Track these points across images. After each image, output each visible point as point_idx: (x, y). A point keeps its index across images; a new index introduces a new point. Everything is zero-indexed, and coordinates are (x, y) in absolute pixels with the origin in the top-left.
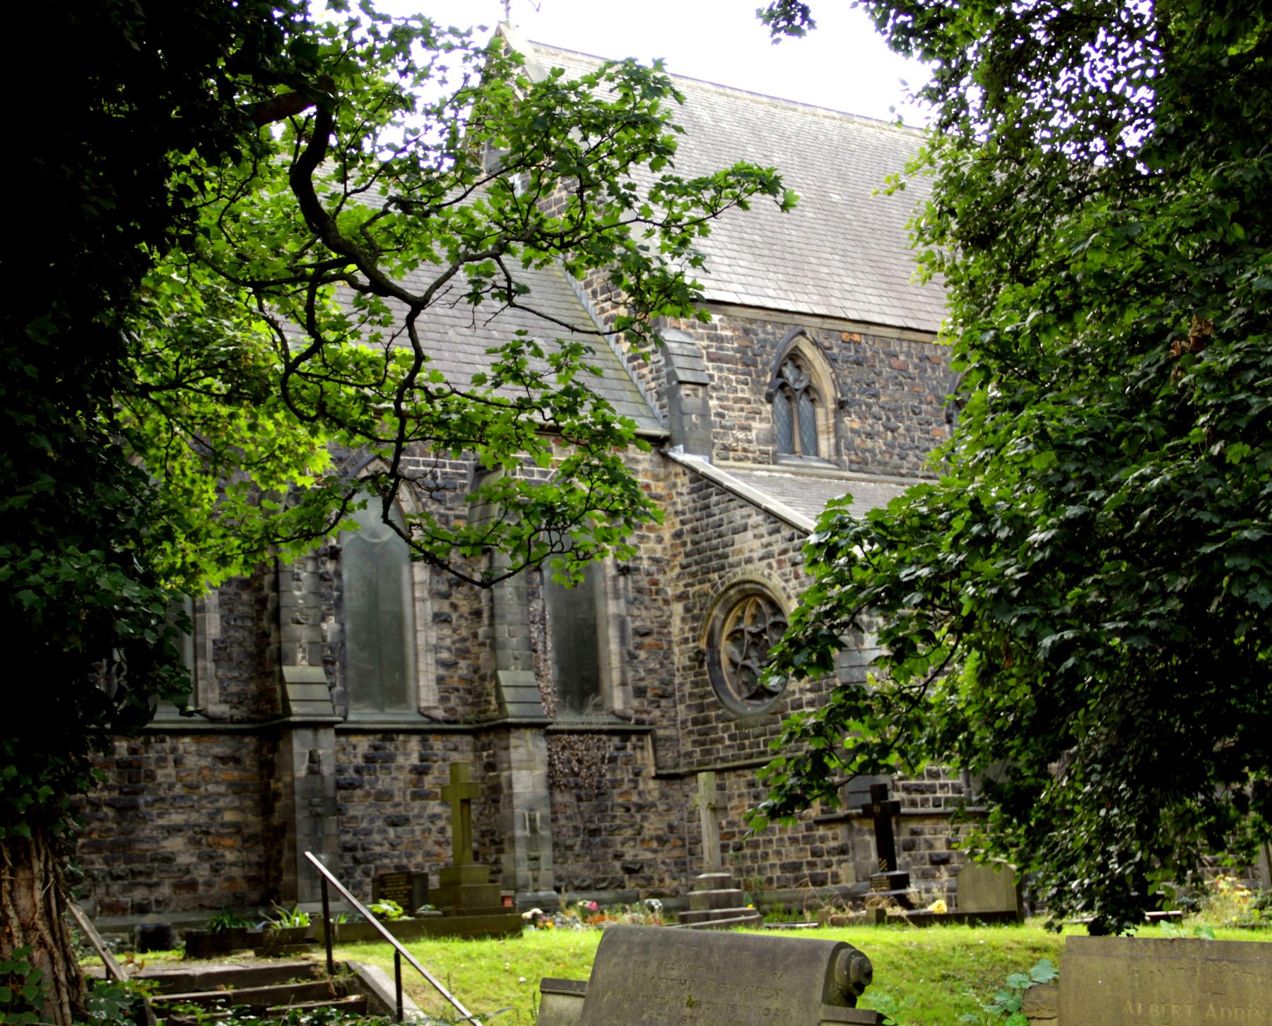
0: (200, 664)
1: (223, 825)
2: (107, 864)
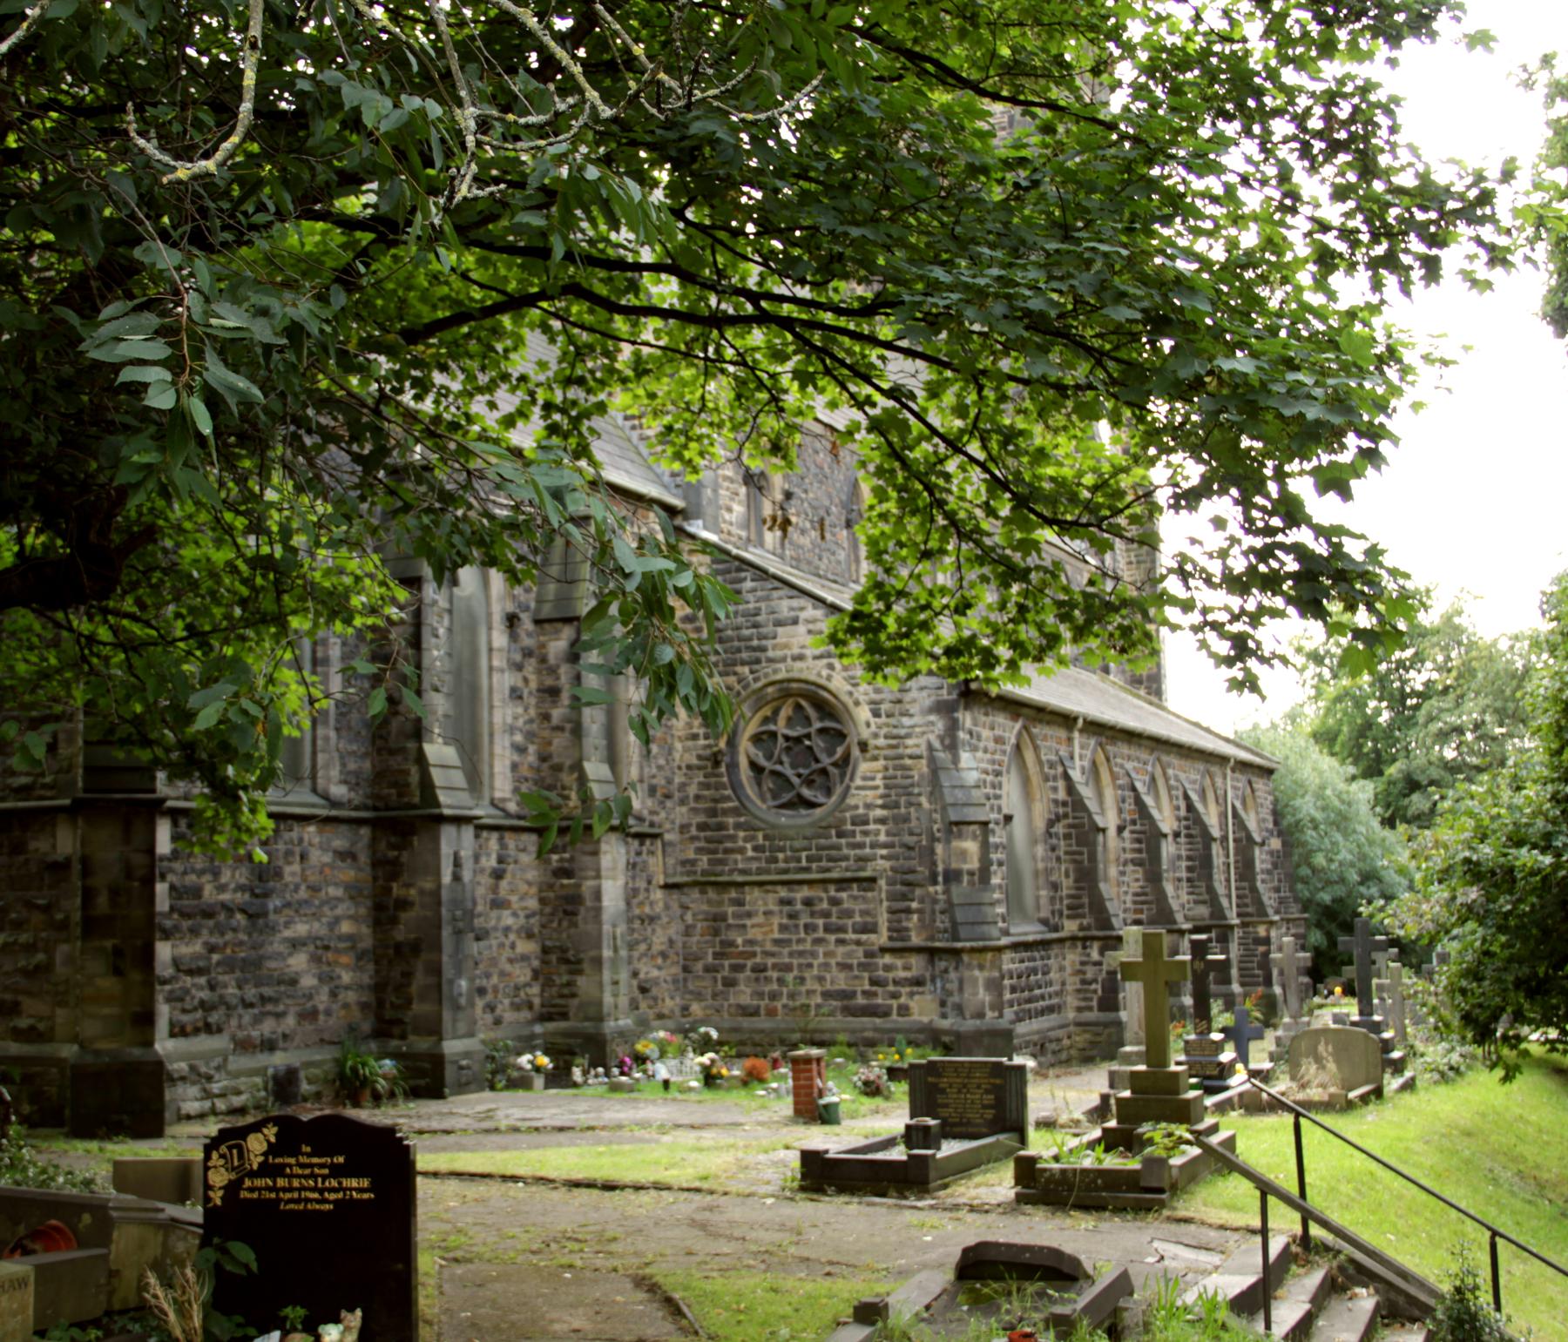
0: (320, 731)
1: (341, 938)
2: (240, 987)
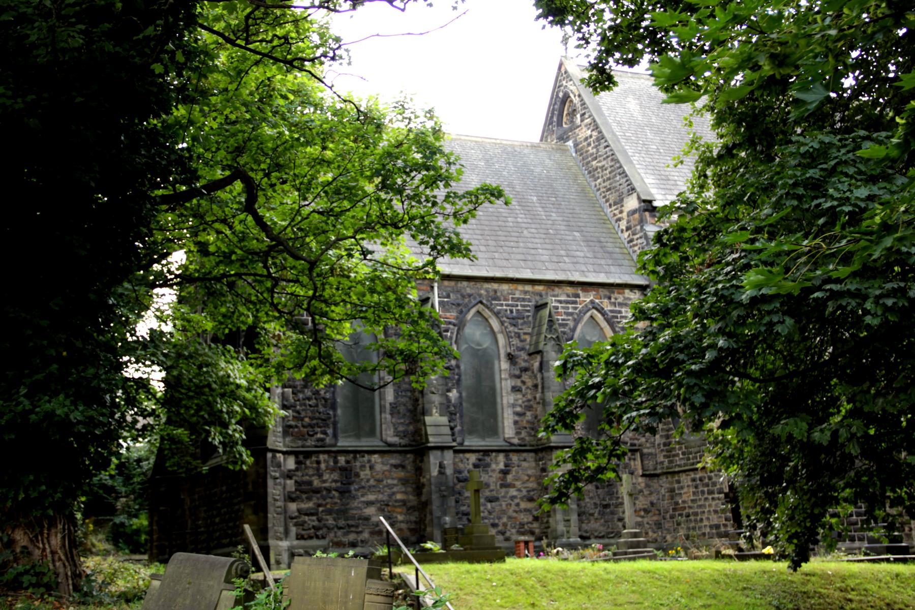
0: (383, 416)
1: (396, 501)
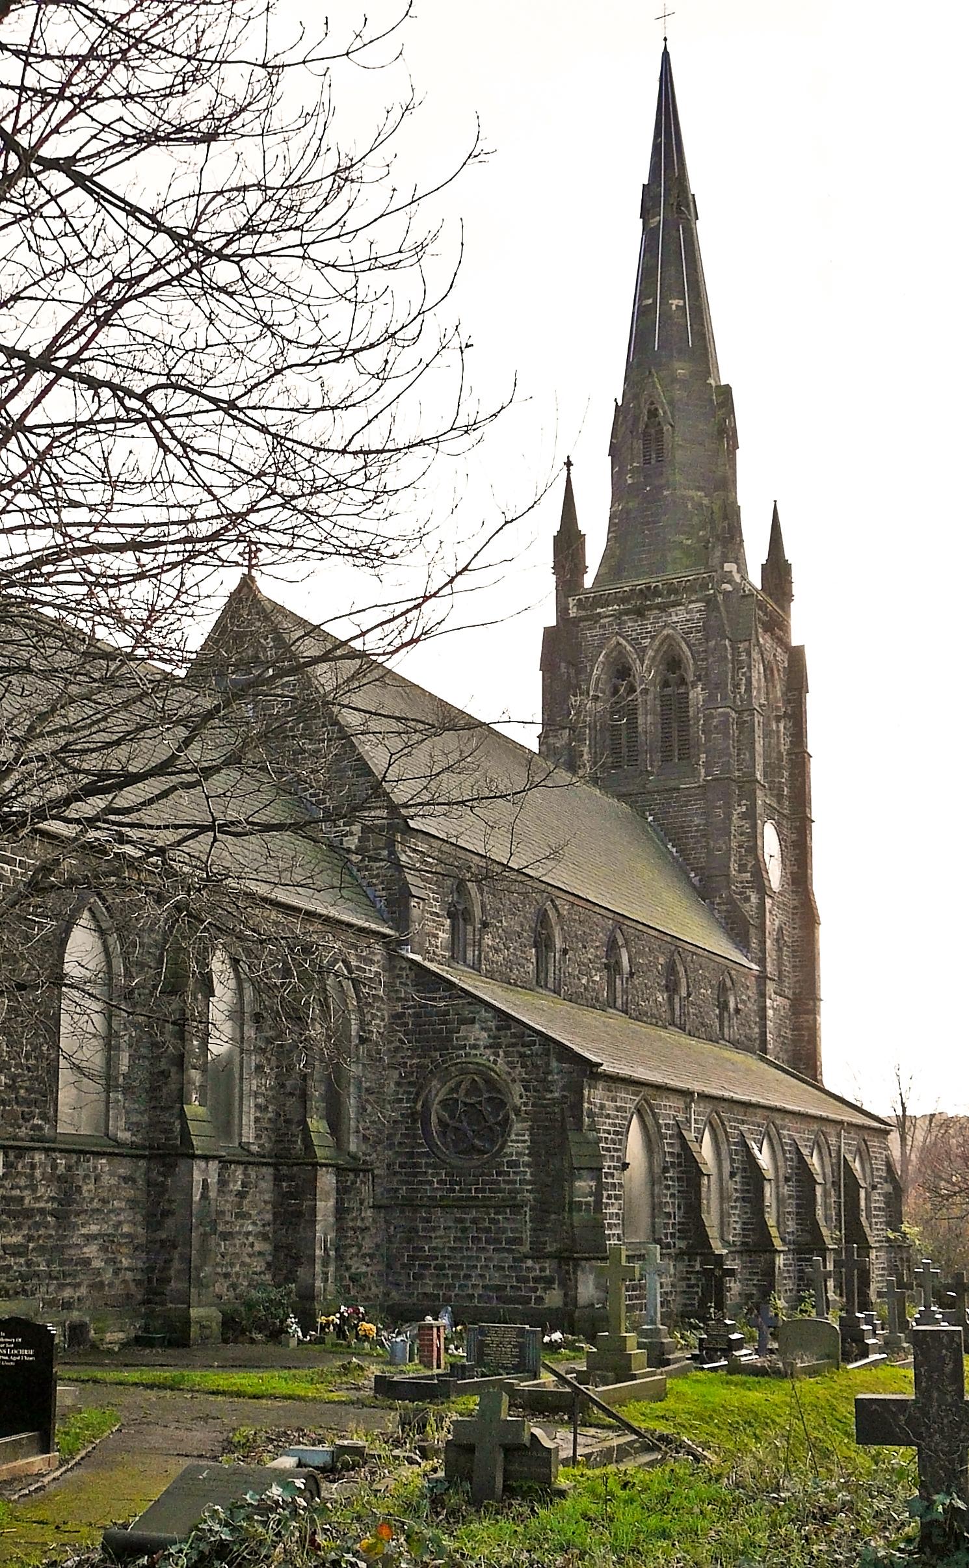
1: (123, 1235)
